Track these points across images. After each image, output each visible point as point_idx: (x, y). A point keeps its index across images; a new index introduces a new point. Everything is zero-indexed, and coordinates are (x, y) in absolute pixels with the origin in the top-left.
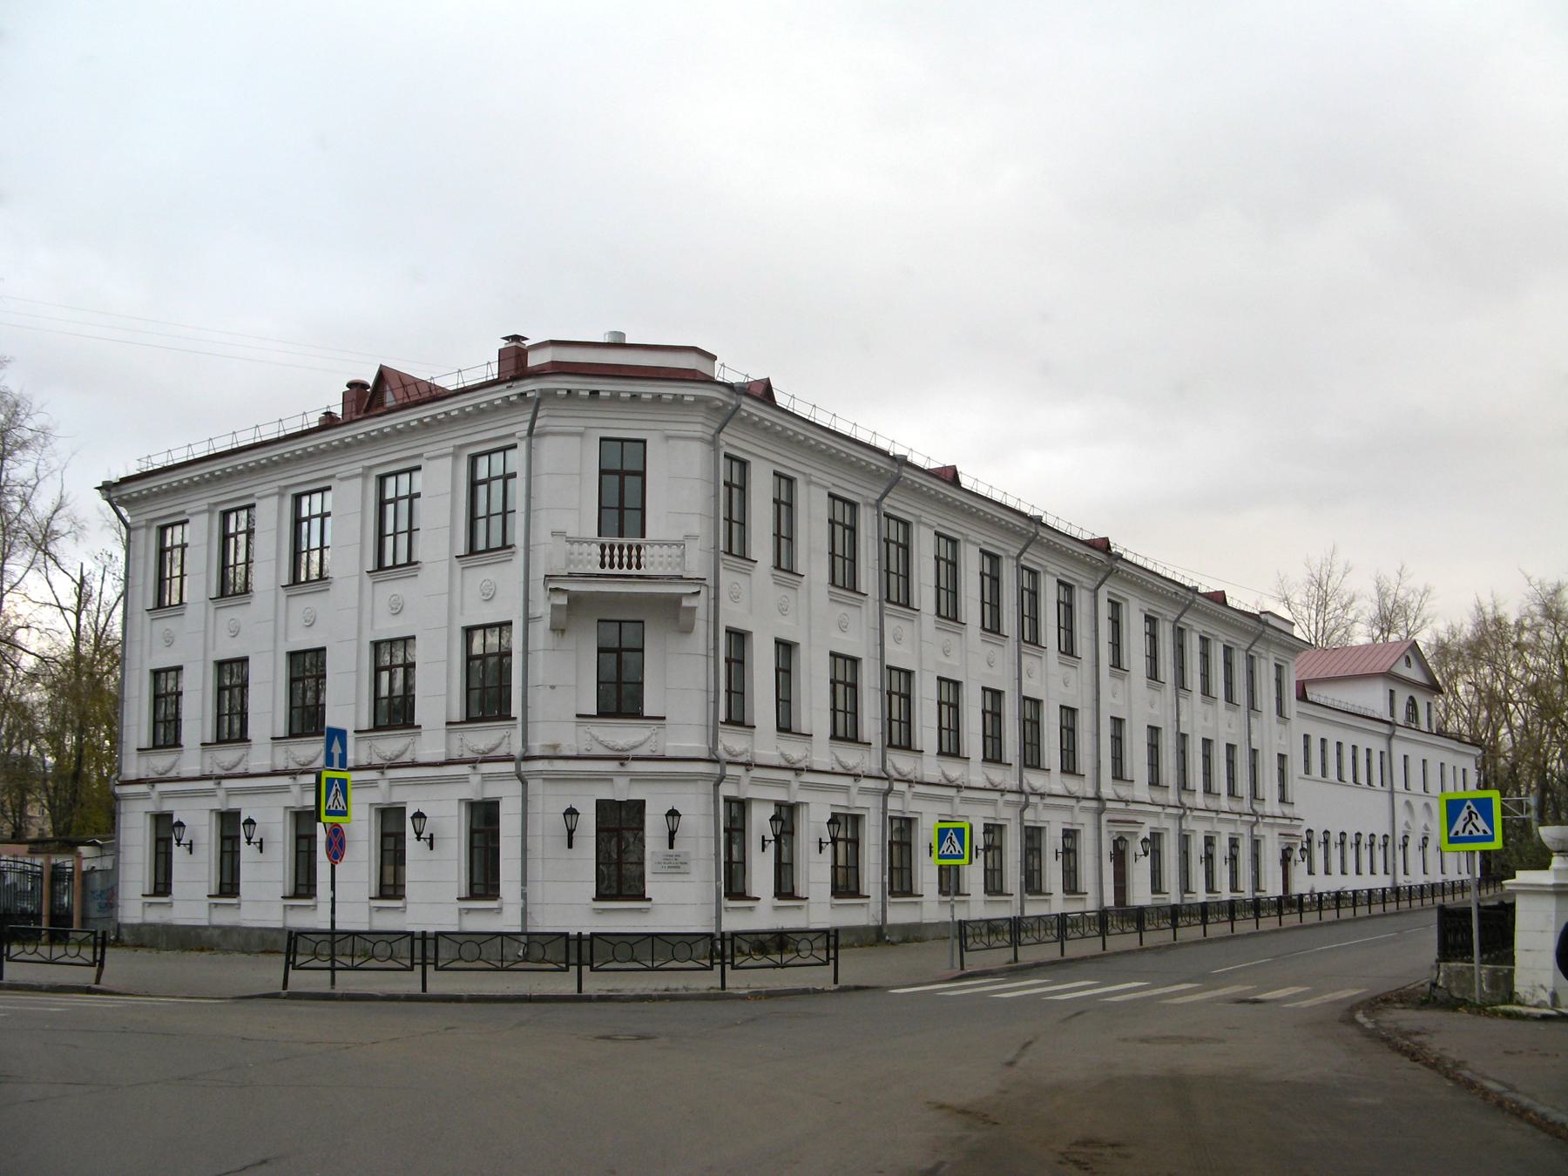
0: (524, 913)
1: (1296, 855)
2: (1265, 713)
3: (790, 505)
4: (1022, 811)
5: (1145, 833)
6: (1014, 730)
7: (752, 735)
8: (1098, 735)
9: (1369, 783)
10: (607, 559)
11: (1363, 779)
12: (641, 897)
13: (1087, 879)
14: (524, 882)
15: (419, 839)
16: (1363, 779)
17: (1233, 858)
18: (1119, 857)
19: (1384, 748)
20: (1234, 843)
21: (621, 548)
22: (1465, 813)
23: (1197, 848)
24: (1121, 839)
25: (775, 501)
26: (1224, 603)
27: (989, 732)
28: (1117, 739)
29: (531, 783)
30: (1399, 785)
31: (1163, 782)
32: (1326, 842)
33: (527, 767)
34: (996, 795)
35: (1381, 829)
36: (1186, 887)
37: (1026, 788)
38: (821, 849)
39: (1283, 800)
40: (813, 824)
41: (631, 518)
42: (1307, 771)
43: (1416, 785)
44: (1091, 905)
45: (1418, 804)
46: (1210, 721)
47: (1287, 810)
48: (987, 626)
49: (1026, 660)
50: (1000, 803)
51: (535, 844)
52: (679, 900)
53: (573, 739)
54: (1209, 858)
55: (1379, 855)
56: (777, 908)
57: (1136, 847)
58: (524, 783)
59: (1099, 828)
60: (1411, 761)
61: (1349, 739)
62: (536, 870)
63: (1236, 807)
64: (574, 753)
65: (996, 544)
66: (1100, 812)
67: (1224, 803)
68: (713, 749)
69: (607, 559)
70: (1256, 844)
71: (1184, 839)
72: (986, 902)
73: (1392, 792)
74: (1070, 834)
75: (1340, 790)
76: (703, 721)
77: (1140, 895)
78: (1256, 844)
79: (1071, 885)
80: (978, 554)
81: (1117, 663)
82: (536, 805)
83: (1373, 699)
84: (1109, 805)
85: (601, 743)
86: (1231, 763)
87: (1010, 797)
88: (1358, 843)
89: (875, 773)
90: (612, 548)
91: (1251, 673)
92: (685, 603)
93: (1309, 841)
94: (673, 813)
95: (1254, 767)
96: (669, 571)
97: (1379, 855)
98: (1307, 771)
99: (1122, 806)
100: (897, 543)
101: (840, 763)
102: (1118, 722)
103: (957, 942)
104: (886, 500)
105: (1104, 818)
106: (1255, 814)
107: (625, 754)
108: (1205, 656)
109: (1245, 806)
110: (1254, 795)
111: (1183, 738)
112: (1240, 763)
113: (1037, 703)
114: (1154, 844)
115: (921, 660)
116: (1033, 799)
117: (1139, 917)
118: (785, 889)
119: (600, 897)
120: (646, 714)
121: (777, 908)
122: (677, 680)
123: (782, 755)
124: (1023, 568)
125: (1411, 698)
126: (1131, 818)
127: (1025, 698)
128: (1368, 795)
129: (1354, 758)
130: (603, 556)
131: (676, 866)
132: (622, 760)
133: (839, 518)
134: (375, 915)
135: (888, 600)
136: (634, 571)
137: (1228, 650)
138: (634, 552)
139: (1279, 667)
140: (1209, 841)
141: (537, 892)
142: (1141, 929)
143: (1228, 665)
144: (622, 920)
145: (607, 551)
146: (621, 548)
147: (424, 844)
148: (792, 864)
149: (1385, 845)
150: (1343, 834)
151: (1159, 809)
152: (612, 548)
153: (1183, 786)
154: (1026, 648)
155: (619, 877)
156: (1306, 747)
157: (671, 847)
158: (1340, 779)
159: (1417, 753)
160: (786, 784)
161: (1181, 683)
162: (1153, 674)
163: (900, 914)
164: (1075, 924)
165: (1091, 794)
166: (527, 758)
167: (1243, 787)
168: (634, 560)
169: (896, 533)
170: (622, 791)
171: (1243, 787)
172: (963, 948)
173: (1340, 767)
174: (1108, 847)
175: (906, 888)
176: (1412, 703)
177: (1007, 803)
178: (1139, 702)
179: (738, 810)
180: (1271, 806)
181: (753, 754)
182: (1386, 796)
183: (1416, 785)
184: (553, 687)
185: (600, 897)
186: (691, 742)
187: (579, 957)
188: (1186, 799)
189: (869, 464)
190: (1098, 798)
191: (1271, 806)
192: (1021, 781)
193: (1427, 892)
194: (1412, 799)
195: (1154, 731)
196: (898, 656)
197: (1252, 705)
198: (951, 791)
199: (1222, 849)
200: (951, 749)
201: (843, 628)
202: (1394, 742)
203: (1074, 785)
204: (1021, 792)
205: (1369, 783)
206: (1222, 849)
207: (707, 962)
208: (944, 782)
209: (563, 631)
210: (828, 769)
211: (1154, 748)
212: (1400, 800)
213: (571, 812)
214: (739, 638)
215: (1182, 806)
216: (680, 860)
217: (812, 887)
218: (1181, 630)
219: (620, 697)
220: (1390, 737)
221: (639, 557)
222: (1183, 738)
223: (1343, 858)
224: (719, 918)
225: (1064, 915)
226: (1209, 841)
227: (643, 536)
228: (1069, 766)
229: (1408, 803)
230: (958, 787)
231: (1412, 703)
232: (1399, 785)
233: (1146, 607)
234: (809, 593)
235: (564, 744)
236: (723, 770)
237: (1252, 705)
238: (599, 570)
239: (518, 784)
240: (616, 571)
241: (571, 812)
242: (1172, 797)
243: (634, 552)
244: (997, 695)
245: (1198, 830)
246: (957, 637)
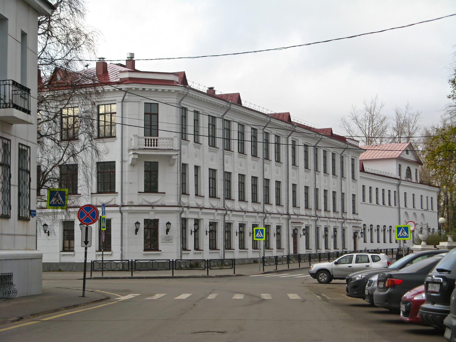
0: (122, 255)
1: (359, 235)
2: (347, 179)
3: (198, 120)
4: (264, 219)
5: (304, 227)
6: (261, 191)
7: (189, 198)
8: (288, 191)
9: (390, 204)
10: (147, 143)
11: (387, 203)
12: (157, 250)
13: (284, 244)
14: (122, 245)
15: (45, 233)
16: (387, 203)
17: (335, 236)
18: (295, 236)
19: (396, 190)
20: (335, 230)
21: (151, 140)
22: (401, 230)
23: (322, 232)
24: (296, 229)
26: (239, 102)
27: (211, 186)
28: (294, 192)
29: (124, 214)
30: (402, 205)
31: (310, 207)
32: (371, 229)
33: (123, 208)
34: (256, 214)
36: (318, 247)
37: (265, 211)
38: (191, 233)
39: (354, 213)
40: (205, 226)
41: (154, 132)
42: (364, 201)
43: (410, 205)
44: (285, 253)
45: (410, 213)
46: (328, 183)
47: (355, 217)
48: (253, 154)
49: (226, 157)
50: (216, 214)
51: (125, 234)
52: (169, 250)
53: (137, 200)
54: (326, 236)
55: (381, 234)
56: (195, 253)
57: (301, 232)
58: (122, 213)
59: (288, 225)
60: (407, 195)
61: (381, 186)
62: (126, 242)
63: (336, 216)
64: (137, 204)
66: (288, 219)
67: (332, 214)
68: (180, 203)
69: (147, 143)
70: (343, 230)
71: (317, 229)
72: (253, 252)
73: (399, 208)
74: (278, 227)
76: (176, 194)
77: (302, 250)
78: (343, 230)
79: (279, 247)
81: (294, 164)
82: (126, 221)
83: (391, 169)
84: (292, 216)
85: (146, 201)
86: (334, 198)
87: (220, 212)
88: (384, 230)
89: (221, 208)
90: (148, 140)
91: (342, 163)
92: (174, 157)
93: (364, 229)
94: (169, 223)
95: (343, 200)
96: (169, 148)
97: (381, 234)
98: (364, 201)
99: (296, 217)
100: (226, 129)
101: (211, 205)
102: (294, 185)
103: (262, 264)
104: (182, 102)
105: (290, 221)
106: (343, 218)
107: (153, 204)
108: (325, 157)
109: (340, 215)
110: (343, 211)
111: (316, 190)
112: (338, 198)
113: (230, 173)
114: (306, 231)
115: (234, 168)
116: (268, 215)
117: (299, 258)
118: (242, 246)
119: (145, 250)
120: (159, 192)
121: (195, 253)
122: (168, 180)
123: (197, 203)
124: (225, 120)
125: (408, 167)
126: (299, 221)
127: (225, 172)
128: (389, 209)
129: (383, 194)
130: (146, 142)
131: (168, 240)
132: (153, 206)
134: (62, 257)
135: (182, 139)
136: (155, 147)
137: (333, 154)
138: (155, 141)
139: (353, 160)
140: (326, 230)
141: (125, 248)
142: (299, 262)
143: (334, 160)
144: (152, 256)
145: (147, 141)
146: (151, 140)
147: (47, 234)
148: (198, 239)
150: (378, 226)
151: (308, 218)
152: (148, 140)
153: (317, 208)
155: (151, 243)
156: (364, 190)
157: (167, 234)
158: (377, 203)
159: (410, 192)
160: (198, 213)
161: (316, 170)
162: (306, 167)
163: (229, 256)
164: (280, 260)
165: (285, 213)
166: (123, 206)
167: (339, 208)
168: (155, 144)
170: (152, 216)
171: (339, 208)
172: (264, 265)
173: (377, 198)
174: (291, 232)
175: (229, 247)
176: (409, 170)
178: (301, 178)
179: (184, 221)
180: (349, 215)
181: (189, 204)
182: (397, 210)
183: (410, 205)
184: (131, 183)
185: (145, 250)
186: (174, 201)
187: (173, 267)
188: (318, 214)
189: (221, 104)
190: (288, 214)
191: (349, 215)
192: (264, 209)
194: (408, 211)
195: (307, 188)
197: (342, 176)
198: (244, 213)
199: (331, 232)
200: (242, 199)
201: (212, 160)
202: (400, 187)
203: (280, 210)
204: (264, 213)
205: (390, 204)
206: (331, 232)
207: (231, 266)
208: (211, 207)
209: (134, 165)
210: (209, 207)
211: (306, 194)
212: (402, 212)
213: (138, 223)
214: (184, 166)
215: (316, 216)
216: (170, 238)
217: (204, 246)
218: (342, 156)
219: (151, 186)
220: (398, 185)
221: (157, 143)
222: (316, 190)
223: (378, 236)
224: (181, 256)
225: (277, 257)
226: (326, 230)
227: (158, 136)
228: (278, 204)
229: (406, 213)
230: (245, 212)
231: (409, 170)
232: (402, 205)
234: (203, 150)
235: (134, 201)
236: (183, 209)
237: (342, 176)
238: (144, 147)
239: (120, 214)
240: (153, 147)
241: (138, 223)
243: (155, 141)
245: (322, 225)
246: (244, 159)
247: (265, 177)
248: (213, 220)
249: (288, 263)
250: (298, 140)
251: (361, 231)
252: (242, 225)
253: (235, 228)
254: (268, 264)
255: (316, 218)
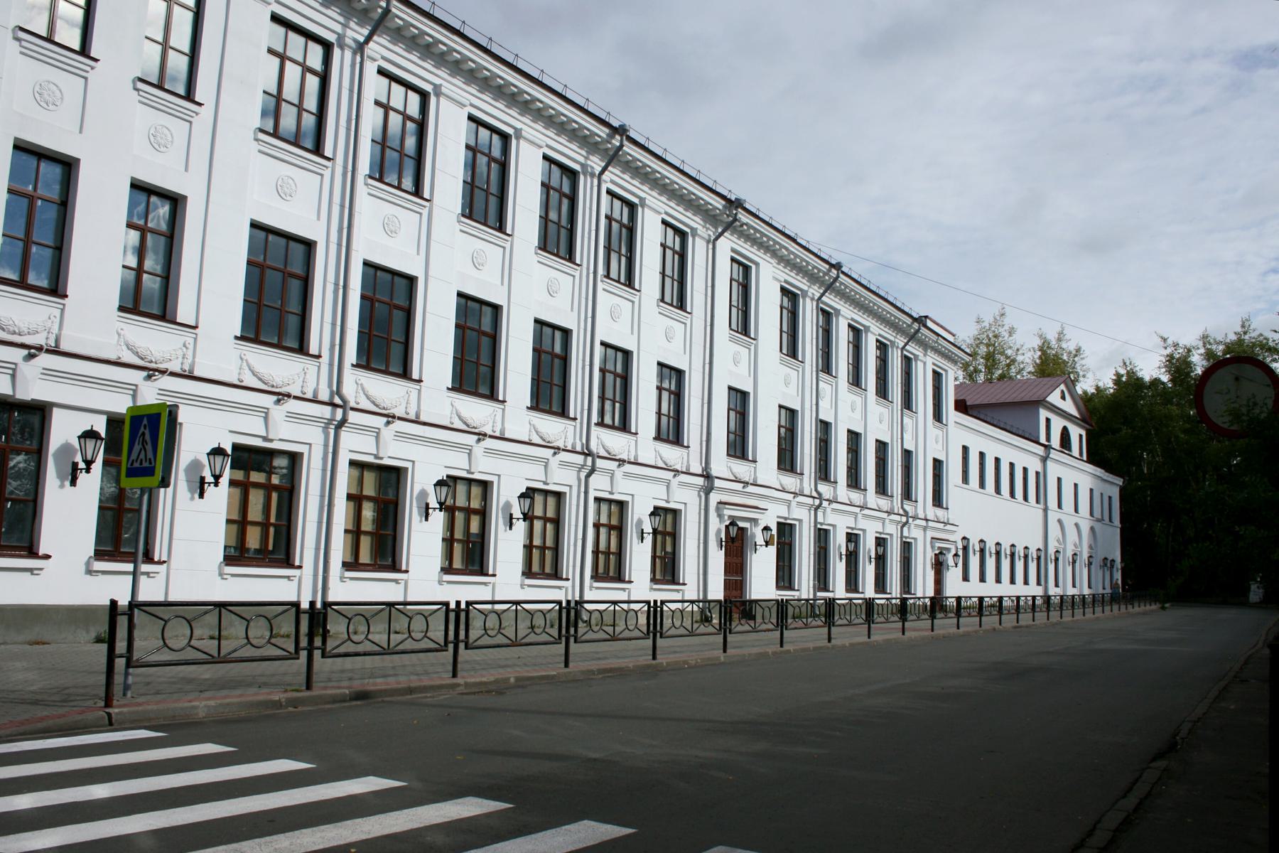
12: (32, 552)
19: (1040, 469)
25: (543, 184)
35: (1035, 543)
48: (734, 326)
55: (1006, 564)
56: (651, 589)
65: (889, 335)
66: (708, 490)
73: (1046, 510)
75: (1011, 504)
80: (660, 227)
97: (1006, 564)
100: (620, 222)
105: (714, 498)
125: (1065, 429)
133: (669, 243)
149: (1039, 558)
154: (822, 375)
169: (620, 211)
177: (563, 464)
182: (1041, 512)
193: (1067, 605)
196: (614, 330)
199: (868, 545)
204: (587, 453)
210: (113, 357)
212: (1053, 516)
233: (783, 277)
242: (808, 483)
244: (792, 413)
247: (821, 417)
248: (265, 439)
249: (933, 617)
250: (757, 264)
251: (953, 552)
252: (852, 538)
253: (839, 541)
254: (882, 619)
255: (904, 519)
